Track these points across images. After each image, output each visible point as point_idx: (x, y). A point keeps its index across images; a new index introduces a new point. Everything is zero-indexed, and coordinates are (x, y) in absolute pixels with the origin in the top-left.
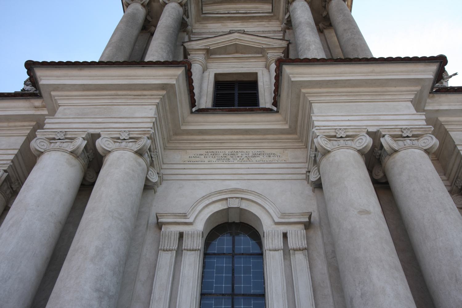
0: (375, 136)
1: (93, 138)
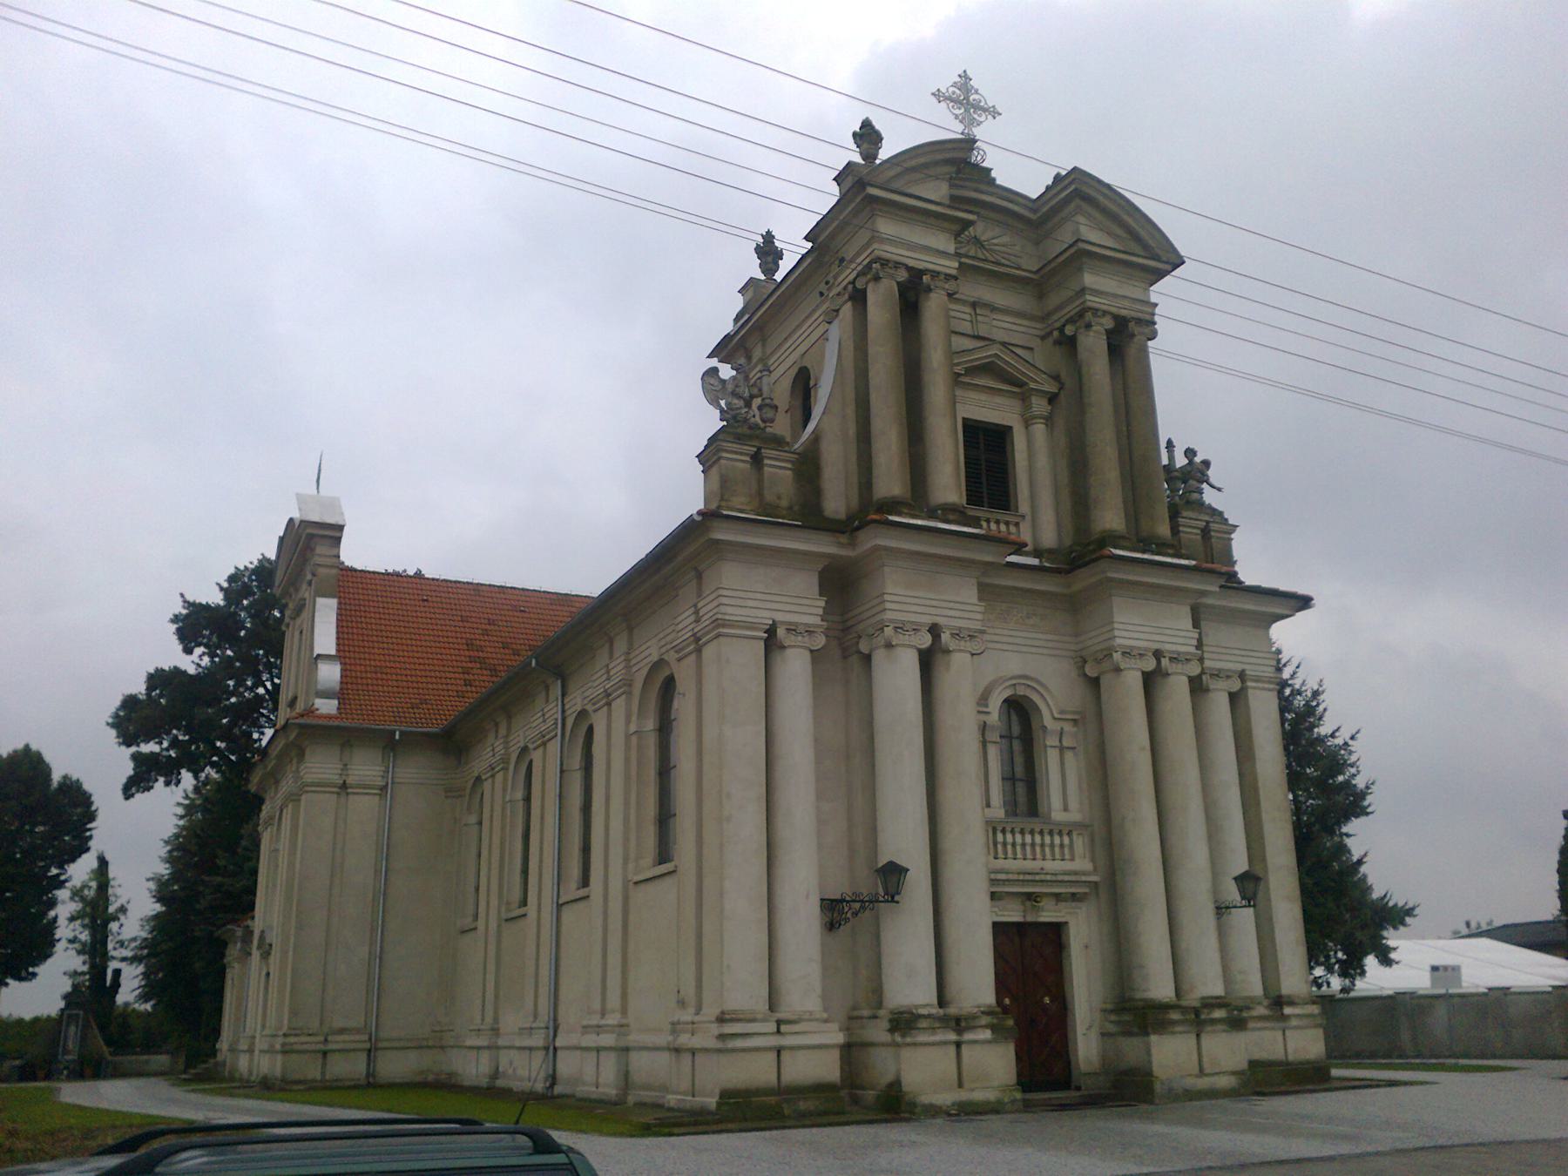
0: (1158, 654)
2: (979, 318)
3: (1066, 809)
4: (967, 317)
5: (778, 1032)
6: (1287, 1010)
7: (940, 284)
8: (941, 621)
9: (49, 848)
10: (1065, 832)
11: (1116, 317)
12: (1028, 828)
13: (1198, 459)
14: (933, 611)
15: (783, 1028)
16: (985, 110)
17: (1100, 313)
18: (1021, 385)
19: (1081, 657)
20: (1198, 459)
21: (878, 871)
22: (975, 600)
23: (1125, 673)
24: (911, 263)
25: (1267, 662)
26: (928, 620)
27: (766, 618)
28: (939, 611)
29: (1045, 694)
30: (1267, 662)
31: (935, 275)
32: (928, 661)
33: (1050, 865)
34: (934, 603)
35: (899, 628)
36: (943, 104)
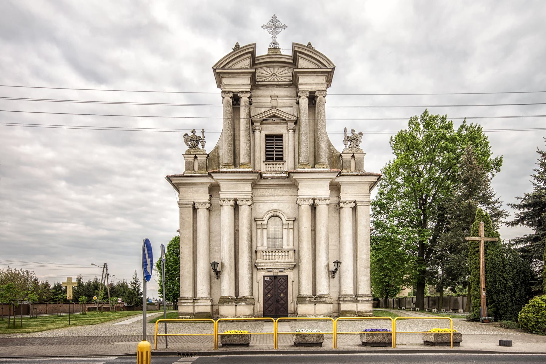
0: (314, 200)
1: (236, 200)
2: (273, 101)
3: (262, 246)
4: (269, 101)
5: (194, 301)
6: (359, 299)
7: (244, 95)
8: (238, 197)
9: (281, 294)
10: (286, 251)
11: (310, 92)
12: (274, 251)
13: (357, 133)
14: (234, 195)
15: (195, 301)
16: (281, 27)
17: (304, 92)
18: (285, 120)
19: (194, 202)
20: (357, 133)
21: (211, 264)
22: (250, 191)
23: (302, 206)
24: (234, 90)
25: (206, 198)
26: (233, 197)
27: (192, 201)
28: (237, 195)
29: (282, 213)
30: (206, 198)
31: (242, 92)
32: (355, 209)
33: (279, 261)
34: (236, 192)
35: (302, 200)
36: (266, 29)
